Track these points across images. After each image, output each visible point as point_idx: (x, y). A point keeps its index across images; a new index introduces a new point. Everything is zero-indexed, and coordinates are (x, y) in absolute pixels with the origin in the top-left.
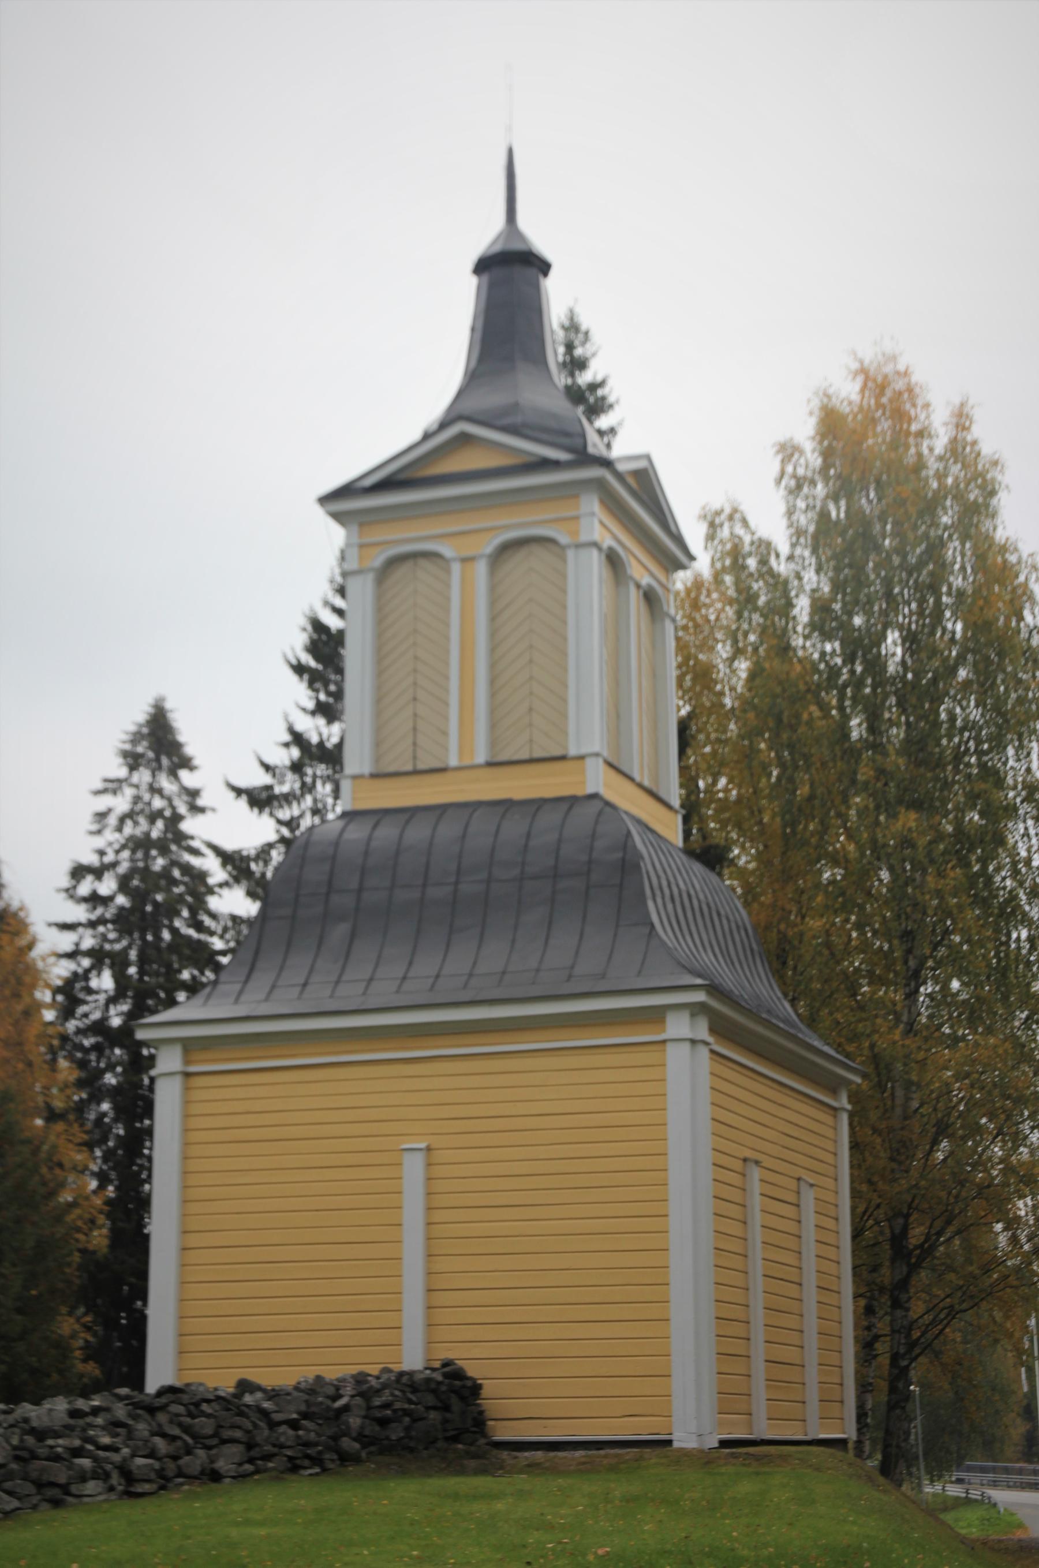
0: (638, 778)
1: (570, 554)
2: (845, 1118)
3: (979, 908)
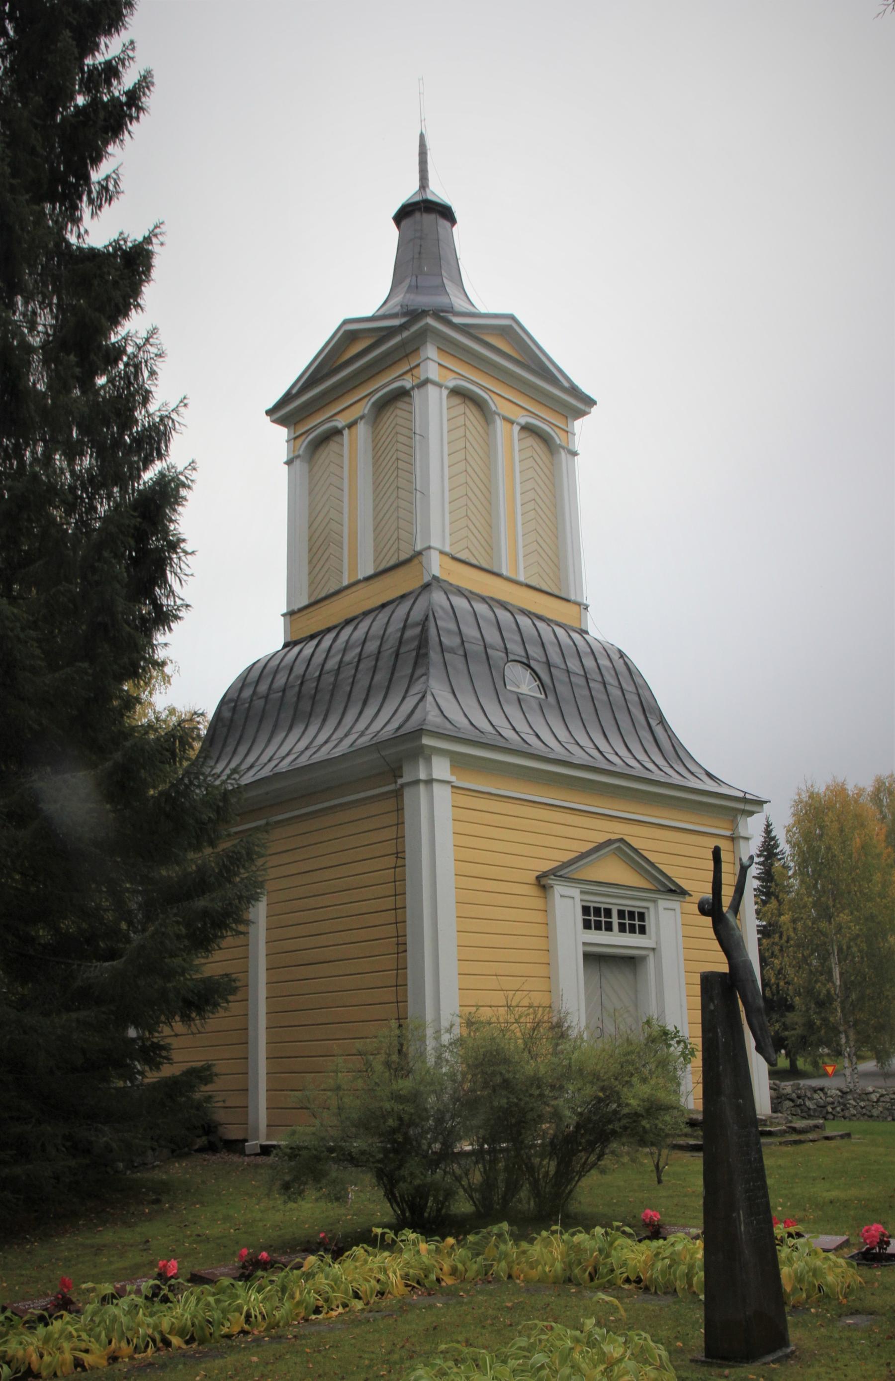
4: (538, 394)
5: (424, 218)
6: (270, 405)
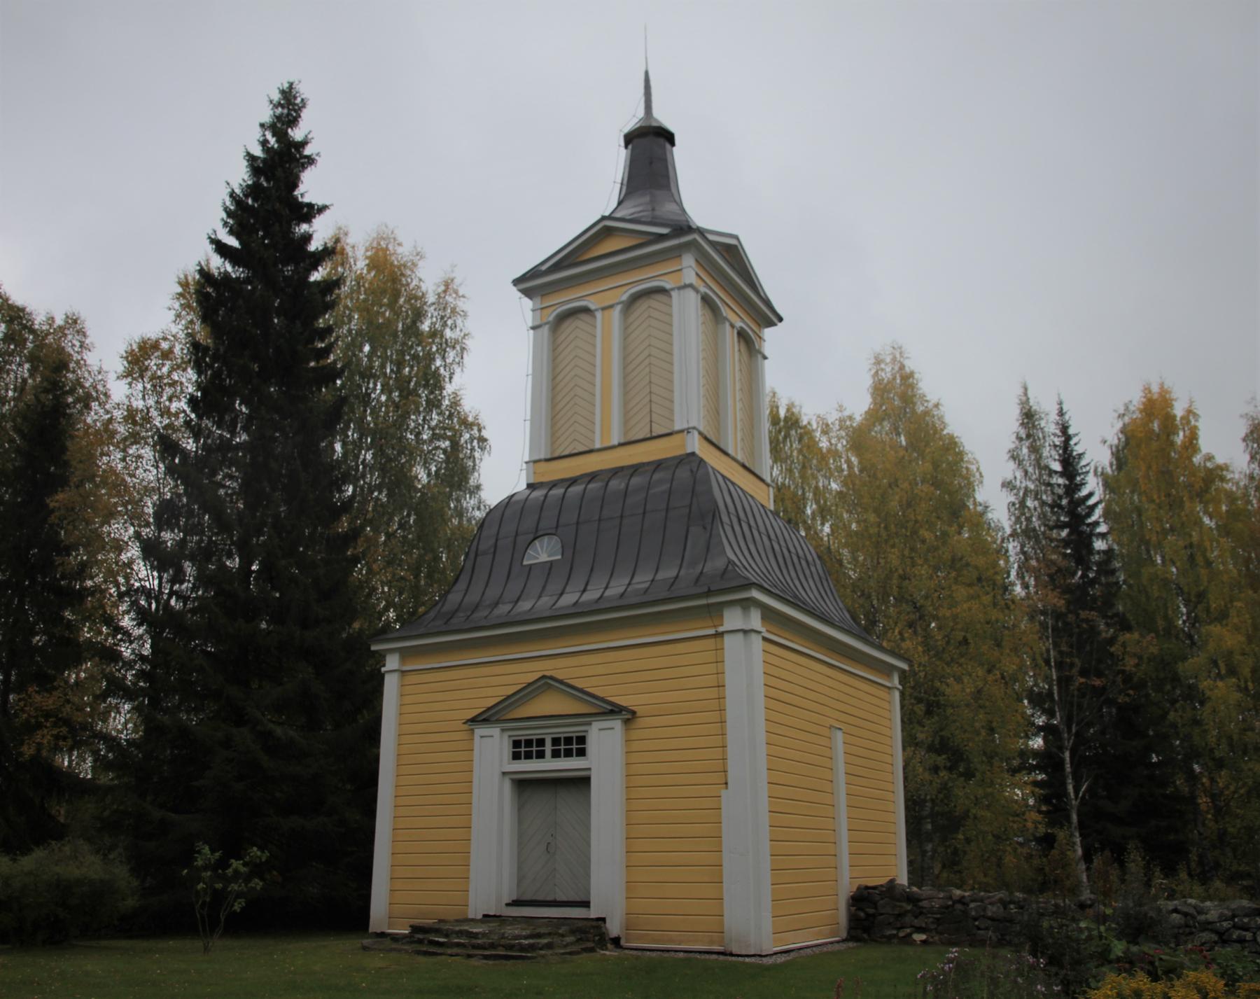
0: (731, 451)
1: (674, 294)
2: (897, 695)
3: (115, 758)
5: (650, 146)
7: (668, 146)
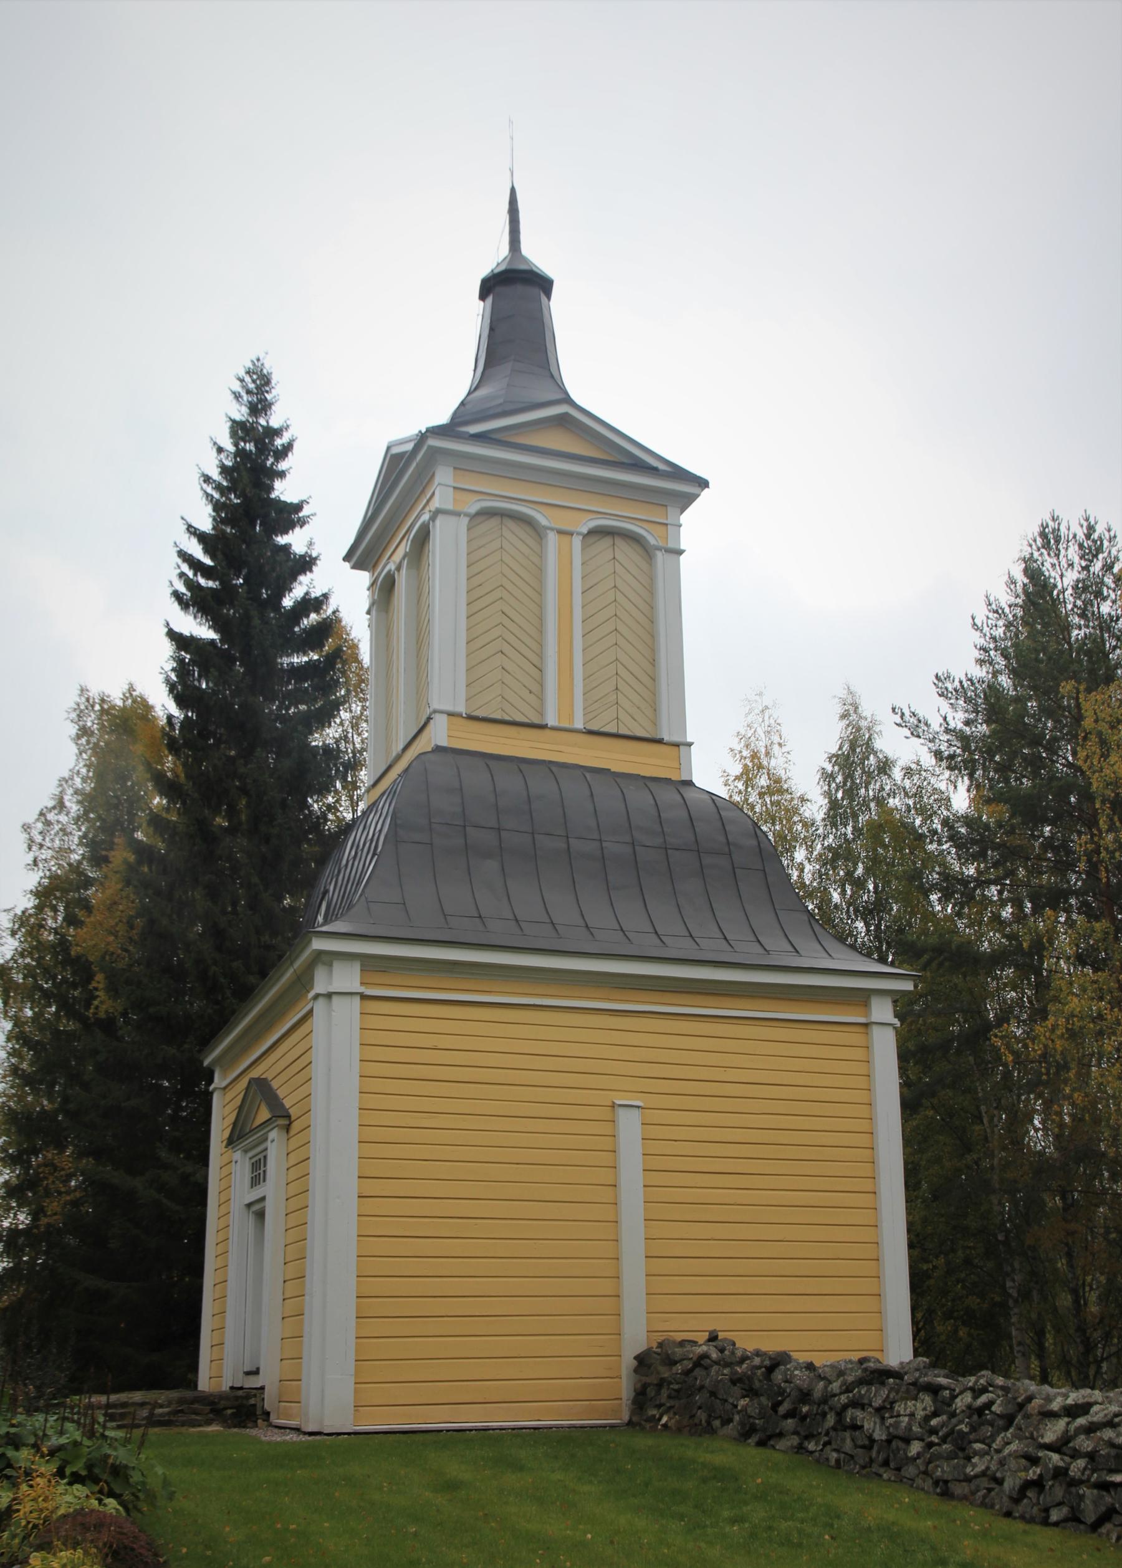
2: (885, 1048)
4: (640, 492)
5: (516, 296)
6: (344, 553)
7: (543, 298)
